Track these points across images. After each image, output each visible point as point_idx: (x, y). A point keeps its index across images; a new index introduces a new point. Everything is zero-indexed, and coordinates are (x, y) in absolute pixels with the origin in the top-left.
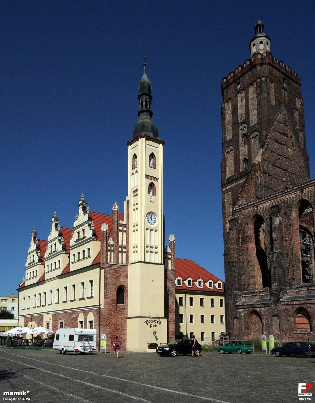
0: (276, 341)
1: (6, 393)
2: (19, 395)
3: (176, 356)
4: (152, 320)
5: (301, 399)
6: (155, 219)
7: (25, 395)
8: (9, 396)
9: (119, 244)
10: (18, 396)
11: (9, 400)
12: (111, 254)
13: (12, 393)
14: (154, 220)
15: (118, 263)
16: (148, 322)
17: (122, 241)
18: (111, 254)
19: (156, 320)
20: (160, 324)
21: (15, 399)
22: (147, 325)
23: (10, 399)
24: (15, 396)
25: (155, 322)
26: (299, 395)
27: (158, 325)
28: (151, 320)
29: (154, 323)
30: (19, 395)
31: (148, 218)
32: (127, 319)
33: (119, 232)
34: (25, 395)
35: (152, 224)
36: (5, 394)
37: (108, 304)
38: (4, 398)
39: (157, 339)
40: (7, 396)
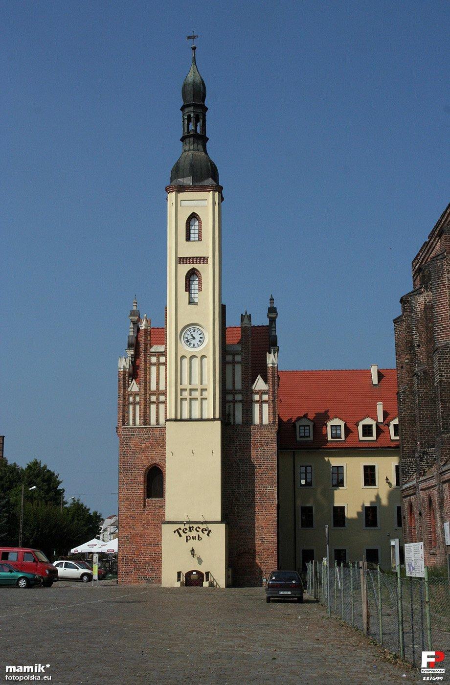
0: (96, 558)
1: (11, 667)
2: (32, 671)
3: (25, 588)
4: (190, 528)
5: (426, 678)
6: (201, 336)
7: (43, 671)
8: (17, 674)
9: (150, 390)
10: (31, 674)
11: (16, 680)
12: (134, 409)
13: (20, 669)
14: (201, 338)
15: (150, 425)
16: (181, 532)
17: (158, 383)
18: (134, 409)
19: (199, 528)
20: (208, 535)
21: (26, 678)
22: (180, 536)
23: (17, 678)
24: (26, 673)
25: (198, 531)
26: (423, 672)
27: (204, 536)
28: (191, 528)
29: (194, 533)
30: (32, 671)
31: (186, 336)
32: (162, 525)
33: (150, 368)
34: (43, 671)
35: (196, 345)
36: (9, 669)
37: (127, 499)
38: (6, 677)
39: (200, 561)
40: (12, 673)
